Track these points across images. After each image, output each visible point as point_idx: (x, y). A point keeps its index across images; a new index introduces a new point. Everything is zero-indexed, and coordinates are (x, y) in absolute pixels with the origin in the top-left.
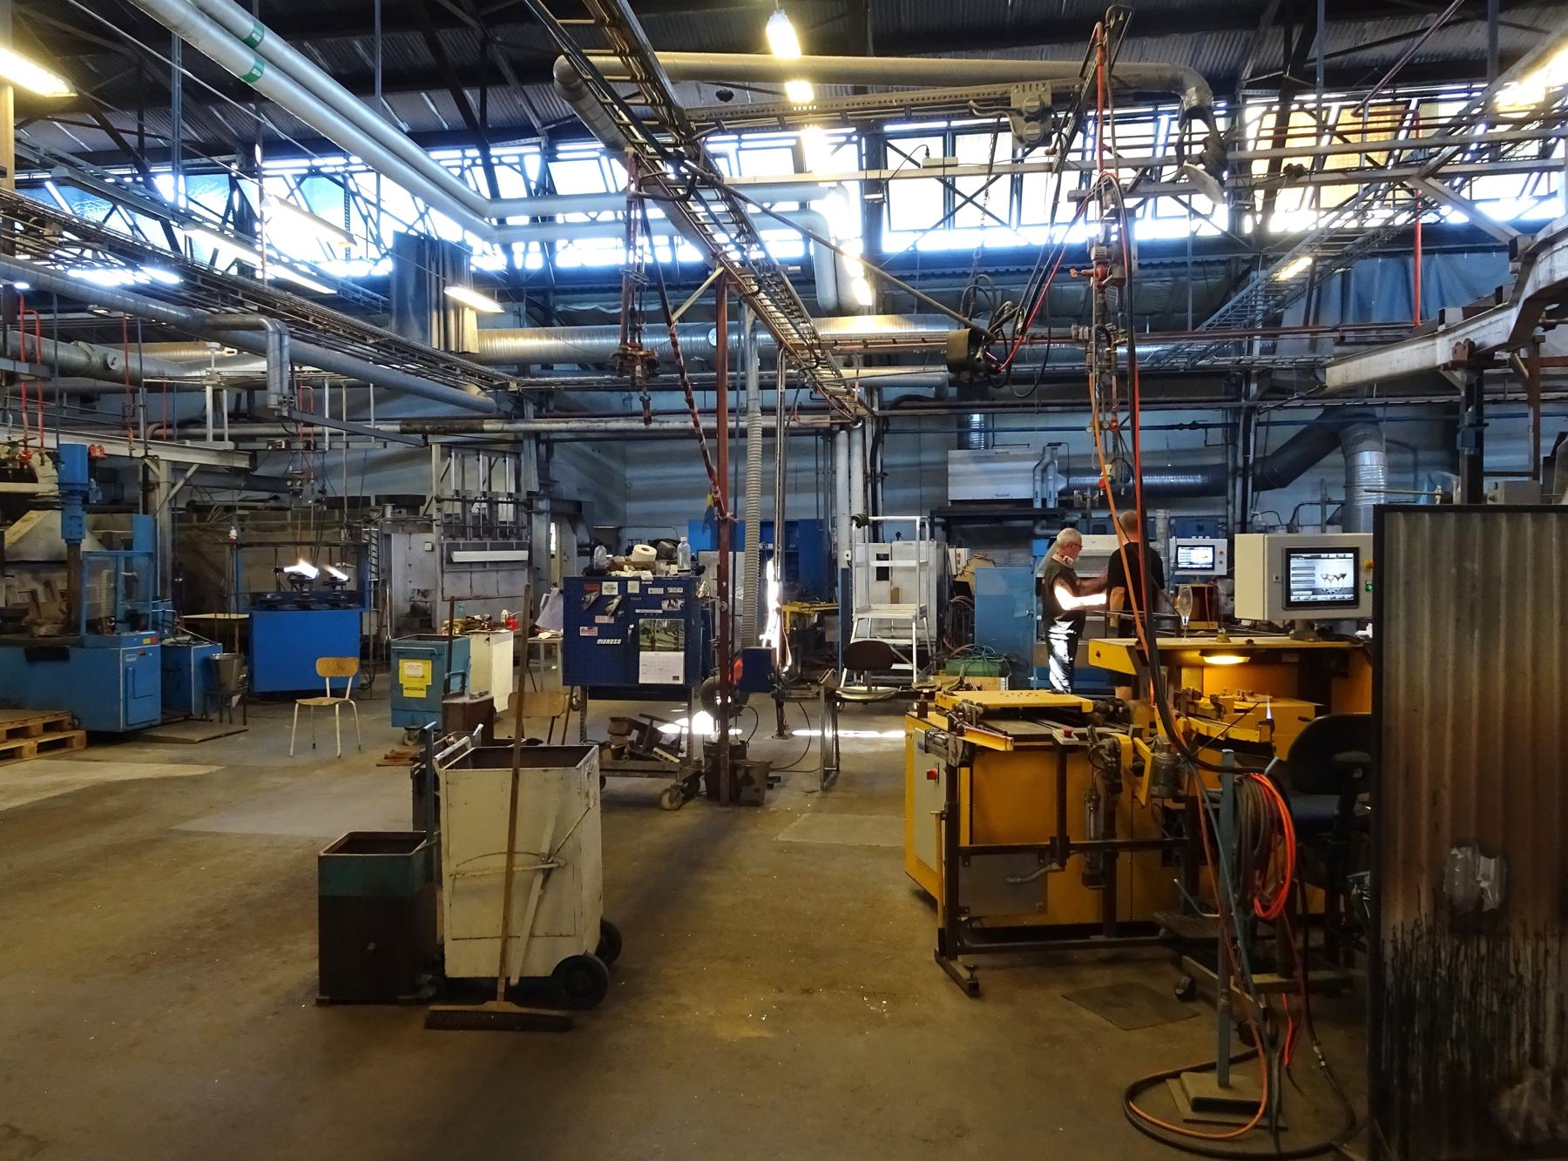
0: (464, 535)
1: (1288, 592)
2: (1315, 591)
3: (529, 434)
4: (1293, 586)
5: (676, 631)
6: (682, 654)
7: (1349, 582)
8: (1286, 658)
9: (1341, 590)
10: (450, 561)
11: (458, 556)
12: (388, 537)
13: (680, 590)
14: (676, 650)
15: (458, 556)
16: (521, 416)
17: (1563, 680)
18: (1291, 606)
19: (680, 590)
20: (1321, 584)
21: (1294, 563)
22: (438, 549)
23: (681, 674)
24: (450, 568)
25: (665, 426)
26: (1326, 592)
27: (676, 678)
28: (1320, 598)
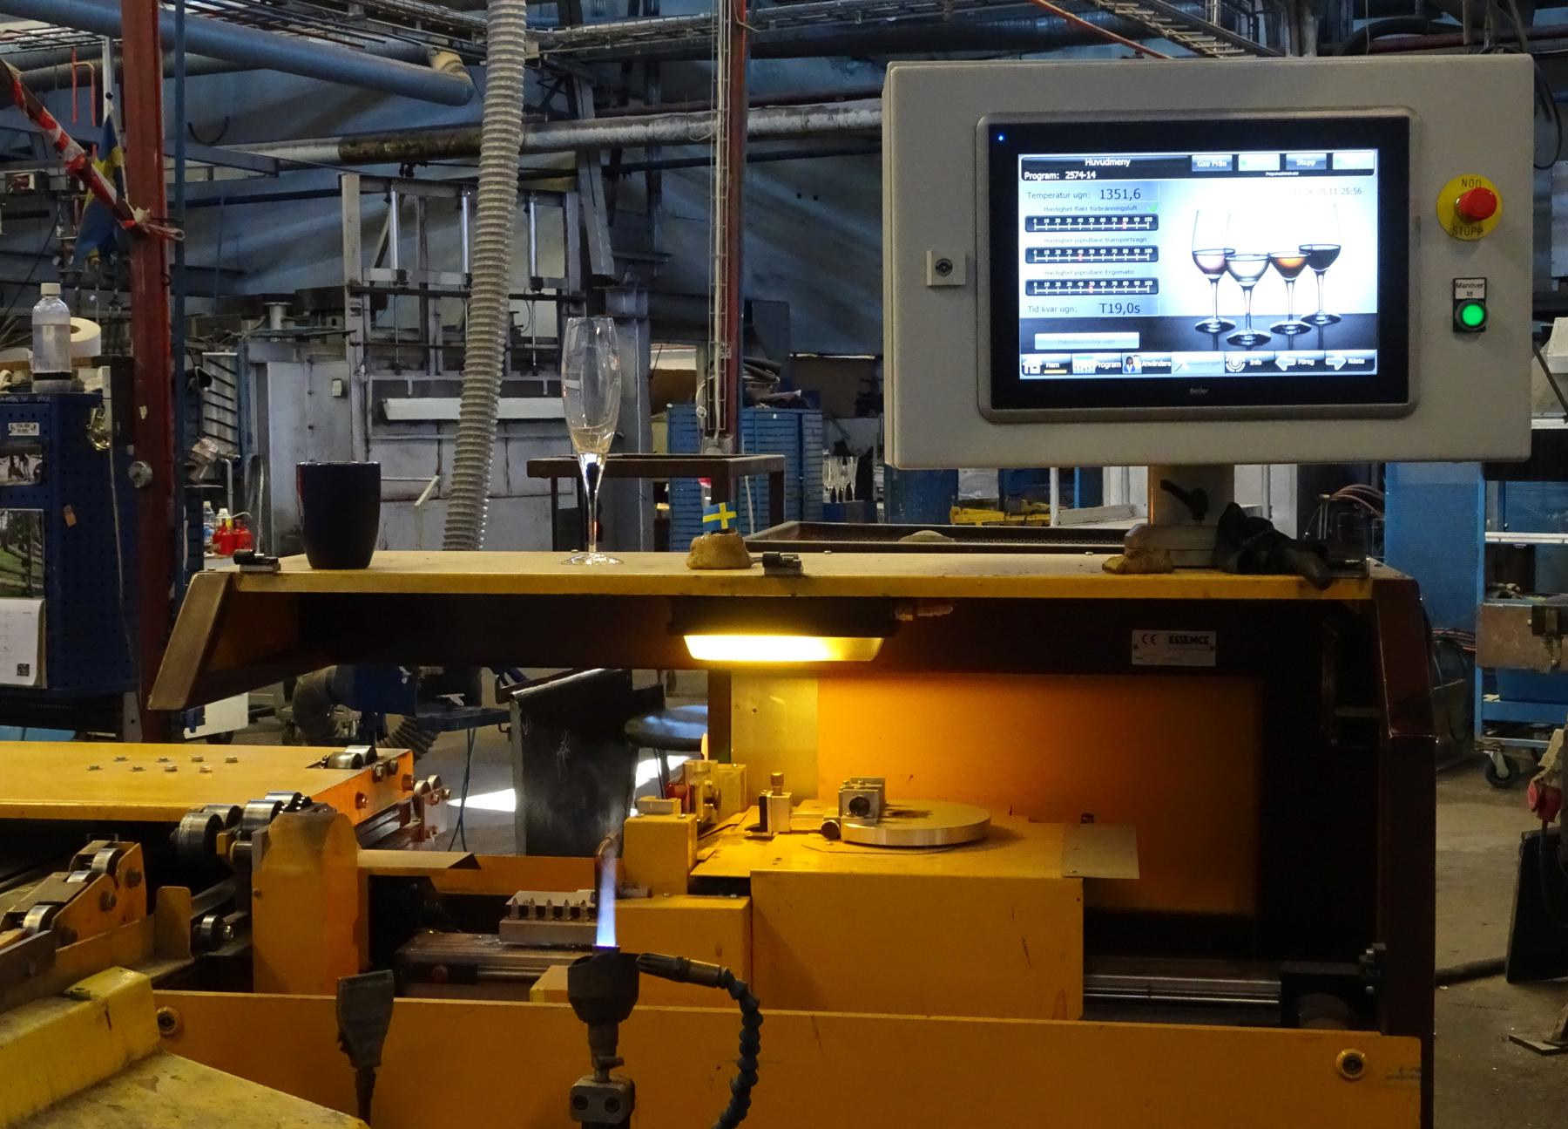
0: (424, 366)
1: (1005, 334)
2: (1157, 334)
3: (588, 152)
4: (1029, 307)
5: (24, 542)
6: (35, 604)
7: (1354, 288)
8: (1149, 648)
9: (1309, 329)
10: (381, 418)
11: (398, 408)
12: (261, 367)
13: (33, 430)
14: (26, 593)
15: (398, 408)
16: (571, 115)
17: (668, 910)
18: (1013, 396)
19: (33, 430)
20: (1183, 295)
21: (1036, 195)
22: (355, 393)
23: (32, 660)
24: (382, 433)
25: (841, 119)
26: (1222, 336)
27: (23, 670)
28: (1185, 364)
